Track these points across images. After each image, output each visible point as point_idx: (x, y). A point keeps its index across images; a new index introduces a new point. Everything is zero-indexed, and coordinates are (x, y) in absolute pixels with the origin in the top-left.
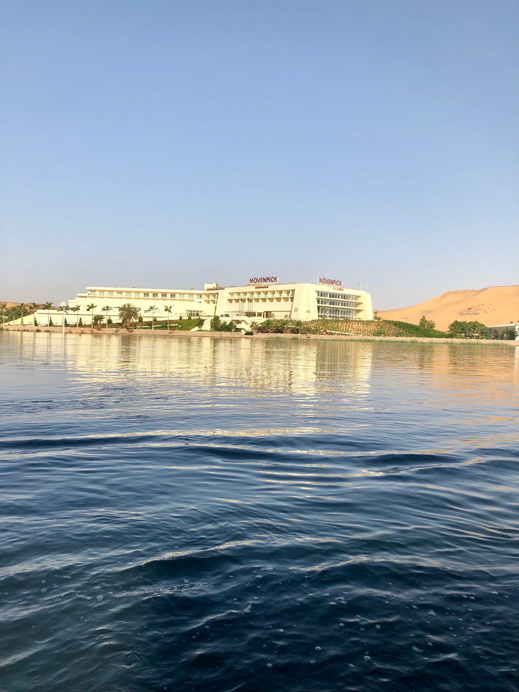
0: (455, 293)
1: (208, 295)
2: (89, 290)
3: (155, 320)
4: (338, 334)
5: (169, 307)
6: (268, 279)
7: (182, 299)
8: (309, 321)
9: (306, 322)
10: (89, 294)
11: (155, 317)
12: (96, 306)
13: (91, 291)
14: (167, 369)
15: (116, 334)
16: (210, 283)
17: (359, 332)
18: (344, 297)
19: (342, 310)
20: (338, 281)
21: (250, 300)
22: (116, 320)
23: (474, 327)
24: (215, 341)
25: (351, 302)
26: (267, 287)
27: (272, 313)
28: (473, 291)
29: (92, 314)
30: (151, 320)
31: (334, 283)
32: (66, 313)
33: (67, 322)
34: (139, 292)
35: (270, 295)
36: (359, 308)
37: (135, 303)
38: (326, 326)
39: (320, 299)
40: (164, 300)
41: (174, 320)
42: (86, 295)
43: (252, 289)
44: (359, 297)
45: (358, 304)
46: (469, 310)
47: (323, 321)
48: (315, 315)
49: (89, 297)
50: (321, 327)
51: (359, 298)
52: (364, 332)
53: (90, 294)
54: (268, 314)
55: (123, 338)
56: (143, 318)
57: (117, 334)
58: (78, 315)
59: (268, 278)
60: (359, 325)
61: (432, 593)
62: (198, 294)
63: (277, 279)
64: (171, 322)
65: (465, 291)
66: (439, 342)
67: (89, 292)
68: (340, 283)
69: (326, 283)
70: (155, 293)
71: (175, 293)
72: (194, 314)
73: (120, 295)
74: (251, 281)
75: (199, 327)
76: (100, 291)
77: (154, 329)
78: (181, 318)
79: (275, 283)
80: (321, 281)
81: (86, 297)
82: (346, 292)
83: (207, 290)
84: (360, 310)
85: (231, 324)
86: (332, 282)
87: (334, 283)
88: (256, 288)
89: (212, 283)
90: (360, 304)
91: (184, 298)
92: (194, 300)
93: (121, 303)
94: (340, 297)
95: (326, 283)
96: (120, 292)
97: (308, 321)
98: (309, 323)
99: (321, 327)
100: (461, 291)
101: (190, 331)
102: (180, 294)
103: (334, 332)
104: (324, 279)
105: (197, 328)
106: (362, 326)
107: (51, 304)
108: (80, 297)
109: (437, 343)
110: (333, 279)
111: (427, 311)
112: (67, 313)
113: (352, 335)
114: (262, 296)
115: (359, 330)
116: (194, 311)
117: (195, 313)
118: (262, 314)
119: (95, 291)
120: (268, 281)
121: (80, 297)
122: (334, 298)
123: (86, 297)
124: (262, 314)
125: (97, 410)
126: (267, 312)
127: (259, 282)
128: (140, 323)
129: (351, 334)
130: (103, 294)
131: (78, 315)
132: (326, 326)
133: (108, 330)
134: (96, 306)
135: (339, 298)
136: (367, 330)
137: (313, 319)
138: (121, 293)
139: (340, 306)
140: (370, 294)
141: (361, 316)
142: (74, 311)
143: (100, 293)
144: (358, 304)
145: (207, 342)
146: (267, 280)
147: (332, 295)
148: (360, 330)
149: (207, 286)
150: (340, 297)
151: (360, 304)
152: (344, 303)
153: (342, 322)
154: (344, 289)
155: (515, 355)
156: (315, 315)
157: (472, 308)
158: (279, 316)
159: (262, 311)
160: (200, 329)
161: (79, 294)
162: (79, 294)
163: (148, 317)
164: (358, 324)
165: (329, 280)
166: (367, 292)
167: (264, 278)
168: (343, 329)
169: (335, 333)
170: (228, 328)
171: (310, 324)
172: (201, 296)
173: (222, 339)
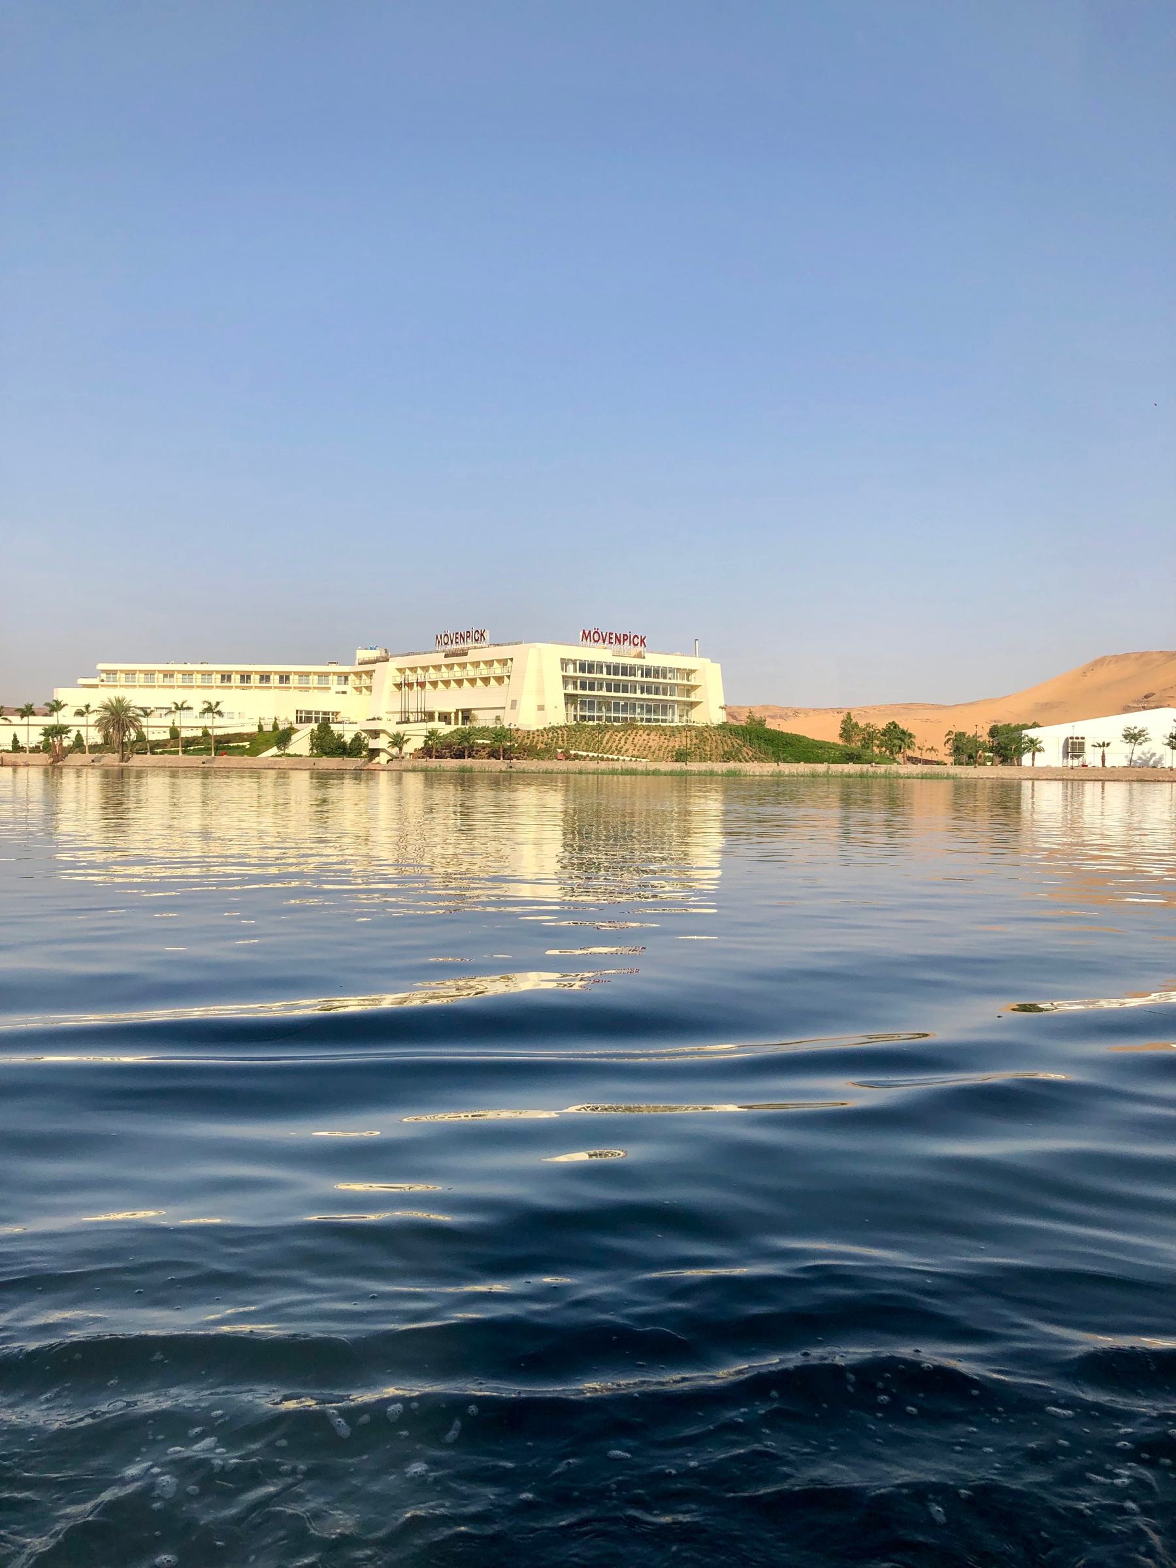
0: (1118, 659)
1: (358, 674)
2: (103, 671)
3: (206, 734)
4: (592, 759)
5: (214, 704)
6: (626, 638)
7: (149, 684)
8: (538, 731)
9: (529, 732)
10: (102, 681)
11: (206, 727)
12: (64, 705)
13: (108, 672)
14: (422, 854)
15: (92, 765)
16: (371, 649)
17: (645, 753)
18: (647, 672)
19: (642, 703)
20: (636, 636)
21: (422, 685)
22: (94, 736)
23: (901, 736)
24: (322, 778)
25: (644, 682)
26: (466, 654)
27: (473, 712)
28: (1161, 654)
29: (86, 724)
30: (199, 733)
31: (624, 640)
32: (8, 723)
33: (18, 742)
34: (210, 673)
35: (471, 672)
36: (693, 698)
37: (136, 698)
38: (573, 740)
39: (577, 678)
40: (243, 688)
41: (246, 734)
42: (96, 681)
43: (439, 658)
44: (693, 671)
45: (690, 689)
46: (1146, 700)
47: (571, 731)
48: (558, 715)
49: (102, 686)
50: (560, 743)
51: (693, 675)
52: (657, 752)
53: (105, 679)
54: (467, 715)
55: (106, 775)
56: (179, 729)
57: (93, 767)
58: (28, 725)
59: (626, 635)
60: (652, 736)
61: (201, 1469)
62: (339, 674)
63: (645, 641)
64: (240, 737)
65: (1142, 655)
66: (555, 770)
67: (104, 676)
68: (642, 641)
69: (601, 641)
70: (226, 674)
71: (268, 672)
72: (301, 717)
73: (168, 682)
74: (438, 640)
75: (279, 748)
76: (185, 673)
77: (30, 753)
78: (260, 727)
79: (483, 644)
80: (586, 636)
81: (96, 686)
82: (653, 660)
83: (359, 664)
84: (697, 702)
85: (357, 738)
86: (621, 639)
87: (624, 640)
88: (446, 656)
89: (375, 649)
90: (694, 687)
91: (192, 682)
92: (329, 688)
93: (99, 698)
94: (605, 670)
95: (601, 641)
96: (169, 674)
97: (535, 729)
98: (537, 733)
99: (560, 743)
100: (1133, 656)
101: (260, 756)
102: (301, 674)
103: (585, 754)
104: (595, 632)
105: (274, 750)
106: (657, 738)
107: (31, 706)
108: (85, 686)
109: (524, 772)
110: (620, 632)
111: (1047, 704)
112: (10, 721)
113: (624, 760)
114: (458, 673)
115: (647, 749)
116: (317, 713)
117: (321, 716)
118: (453, 716)
119: (114, 672)
120: (627, 643)
121: (85, 686)
122: (610, 674)
123: (96, 686)
124: (453, 716)
125: (1158, 961)
126: (464, 711)
127: (604, 642)
128: (172, 742)
129: (621, 758)
130: (133, 680)
131: (28, 725)
132: (573, 740)
133: (76, 758)
134: (64, 705)
135: (601, 672)
136: (666, 748)
137: (552, 725)
138: (172, 676)
139: (638, 695)
140: (719, 665)
141: (698, 718)
142: (22, 717)
143: (301, 678)
144: (690, 689)
145: (301, 782)
146: (467, 637)
147: (614, 669)
148: (650, 747)
149: (362, 654)
150: (605, 670)
151: (694, 687)
152: (663, 689)
153: (617, 730)
154: (647, 655)
155: (1021, 804)
156: (558, 715)
157: (1154, 694)
158: (484, 720)
159: (451, 709)
160: (282, 752)
161: (81, 681)
162: (81, 681)
163: (192, 727)
164: (648, 735)
165: (611, 634)
166: (713, 661)
167: (616, 634)
168: (611, 747)
169: (588, 756)
170: (355, 748)
171: (538, 735)
172: (346, 679)
173: (340, 774)
